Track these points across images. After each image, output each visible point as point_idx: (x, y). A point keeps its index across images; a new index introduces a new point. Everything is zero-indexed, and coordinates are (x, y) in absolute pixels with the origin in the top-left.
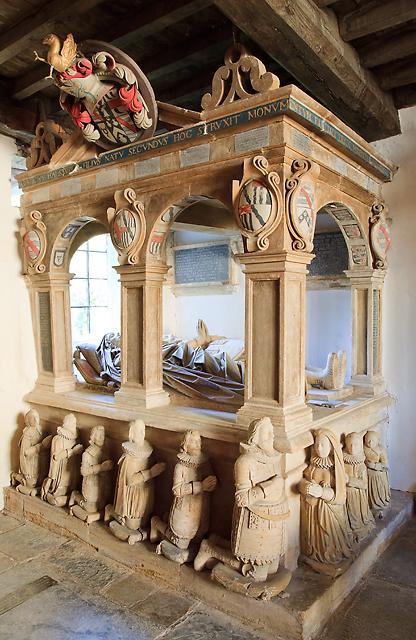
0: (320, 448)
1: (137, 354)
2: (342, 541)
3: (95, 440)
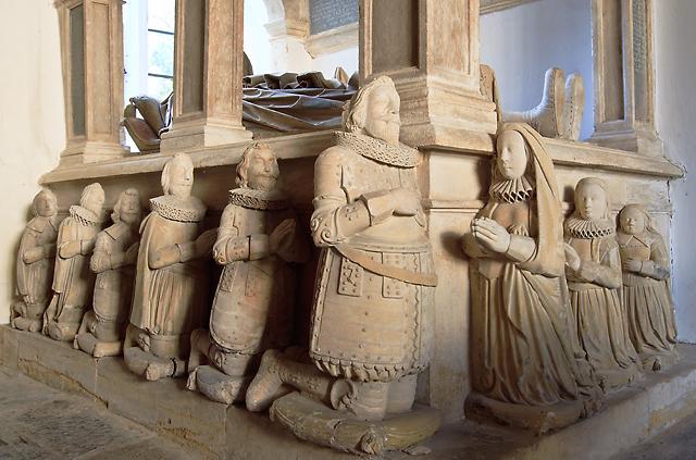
0: (505, 156)
1: (197, 62)
2: (557, 352)
3: (121, 211)
